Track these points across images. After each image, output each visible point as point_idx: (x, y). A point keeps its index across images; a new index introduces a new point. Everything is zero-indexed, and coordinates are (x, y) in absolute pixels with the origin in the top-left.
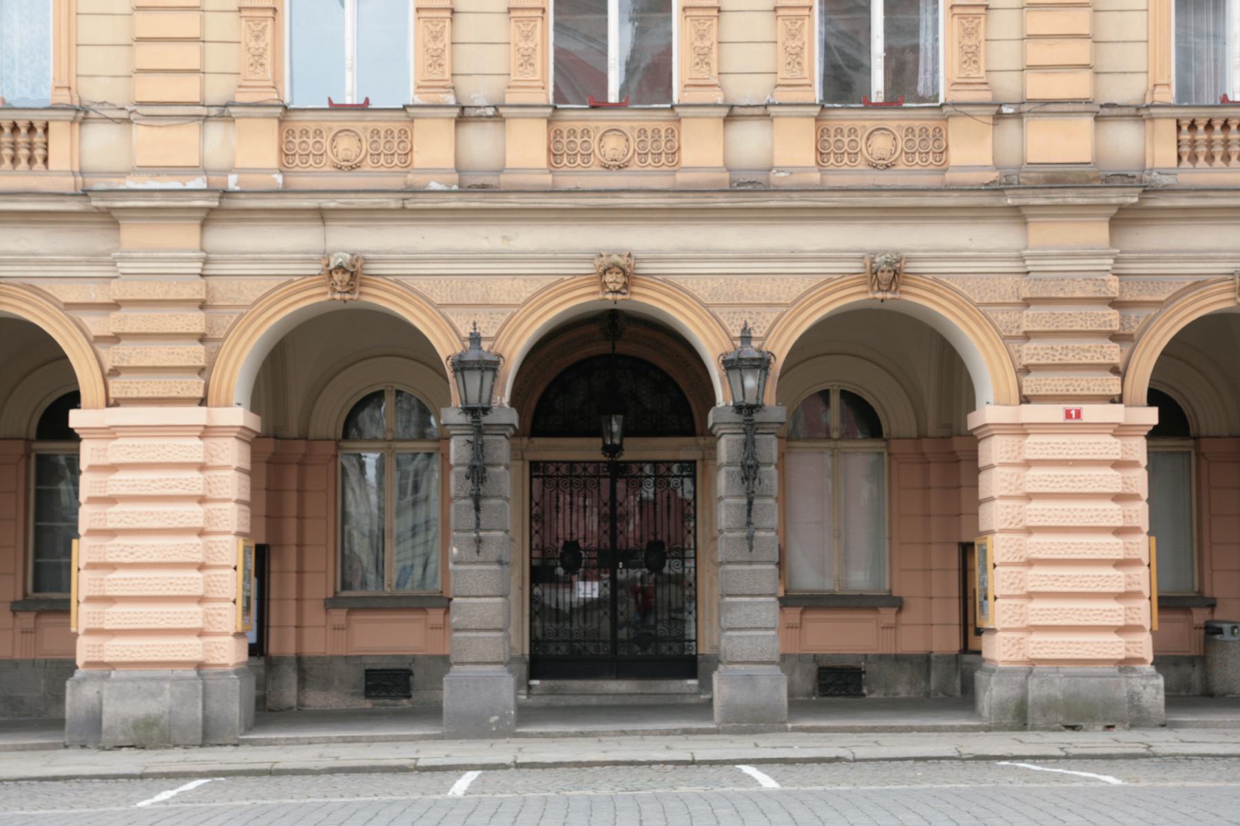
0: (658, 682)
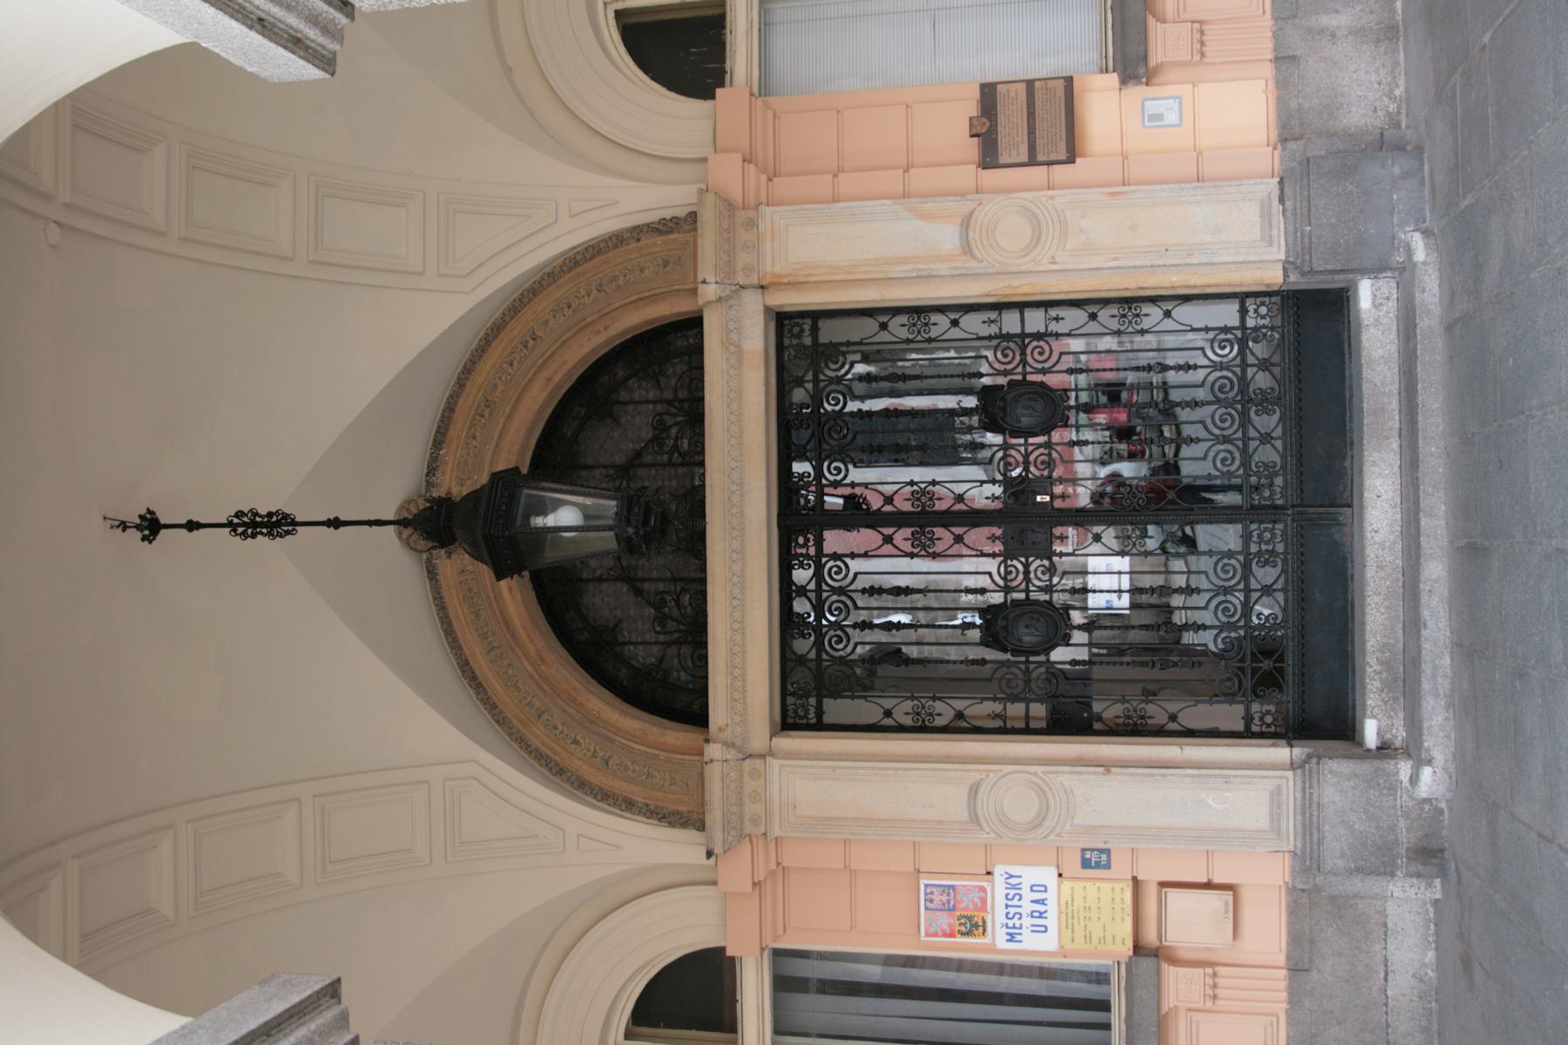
0: (1366, 388)
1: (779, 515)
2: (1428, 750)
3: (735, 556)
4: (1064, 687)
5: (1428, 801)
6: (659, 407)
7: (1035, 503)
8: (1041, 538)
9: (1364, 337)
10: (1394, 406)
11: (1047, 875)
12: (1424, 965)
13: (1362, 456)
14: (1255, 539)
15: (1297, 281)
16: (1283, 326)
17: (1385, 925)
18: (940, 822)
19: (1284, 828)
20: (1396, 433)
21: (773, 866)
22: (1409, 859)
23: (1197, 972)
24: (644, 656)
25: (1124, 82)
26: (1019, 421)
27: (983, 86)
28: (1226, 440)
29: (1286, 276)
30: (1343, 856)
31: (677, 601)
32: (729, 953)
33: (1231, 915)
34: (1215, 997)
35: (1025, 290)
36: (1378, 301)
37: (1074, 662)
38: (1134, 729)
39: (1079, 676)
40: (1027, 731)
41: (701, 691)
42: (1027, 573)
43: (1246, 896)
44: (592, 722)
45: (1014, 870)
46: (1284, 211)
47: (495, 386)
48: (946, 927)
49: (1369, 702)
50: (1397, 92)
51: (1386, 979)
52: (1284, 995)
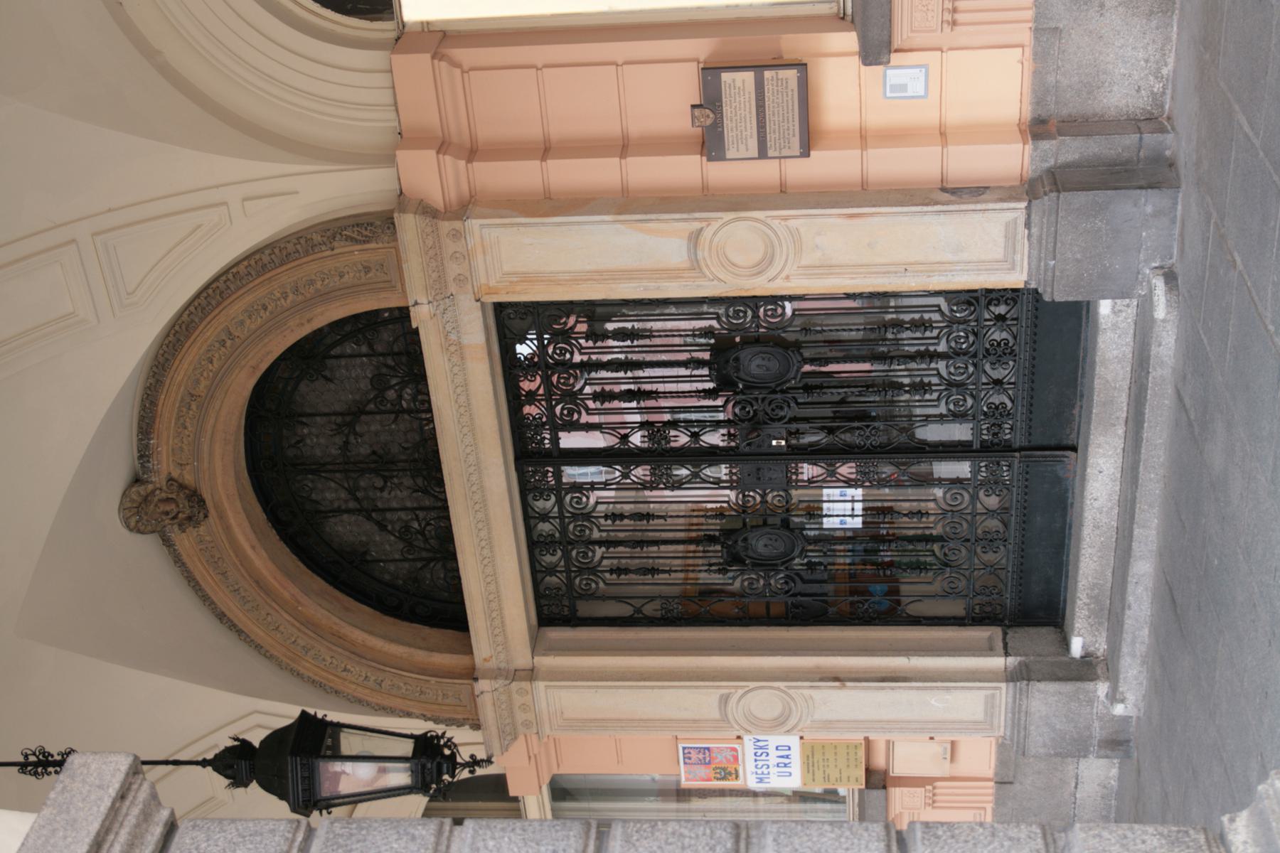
10: (1123, 400)
12: (1108, 778)
19: (996, 722)
20: (1122, 422)
22: (1099, 746)
23: (920, 790)
30: (1045, 745)
46: (1029, 236)
47: (198, 382)
49: (1077, 625)
50: (1165, 71)
51: (1076, 787)
52: (991, 798)
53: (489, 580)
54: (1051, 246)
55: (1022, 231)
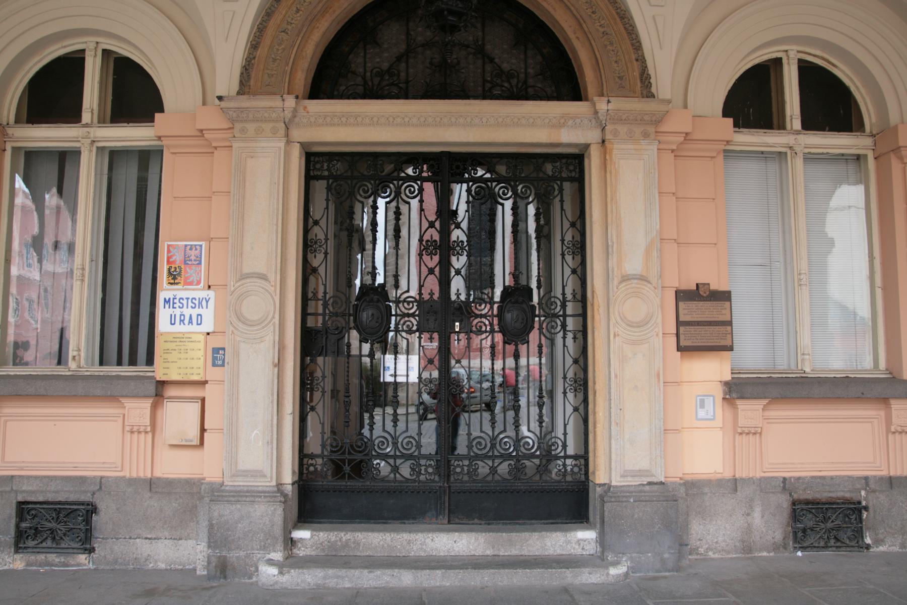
1: (449, 153)
2: (289, 572)
3: (422, 119)
4: (333, 338)
5: (257, 570)
6: (522, 76)
7: (454, 322)
8: (431, 325)
9: (558, 534)
10: (514, 552)
11: (208, 325)
12: (156, 561)
13: (481, 531)
14: (429, 462)
15: (595, 495)
16: (566, 482)
17: (181, 539)
18: (241, 254)
19: (240, 479)
20: (496, 553)
21: (214, 144)
22: (219, 557)
23: (147, 421)
24: (357, 62)
25: (726, 384)
26: (508, 312)
27: (729, 293)
28: (493, 446)
29: (600, 485)
31: (392, 84)
32: (158, 116)
33: (184, 443)
34: (132, 432)
35: (596, 317)
36: (582, 543)
37: (349, 345)
38: (306, 382)
39: (340, 350)
40: (304, 314)
41: (331, 95)
42: (408, 315)
43: (196, 453)
44: (312, 21)
45: (211, 303)
46: (643, 485)
48: (174, 258)
49: (321, 534)
50: (710, 553)
52: (134, 475)
53: (391, 119)
54: (643, 498)
55: (645, 480)
